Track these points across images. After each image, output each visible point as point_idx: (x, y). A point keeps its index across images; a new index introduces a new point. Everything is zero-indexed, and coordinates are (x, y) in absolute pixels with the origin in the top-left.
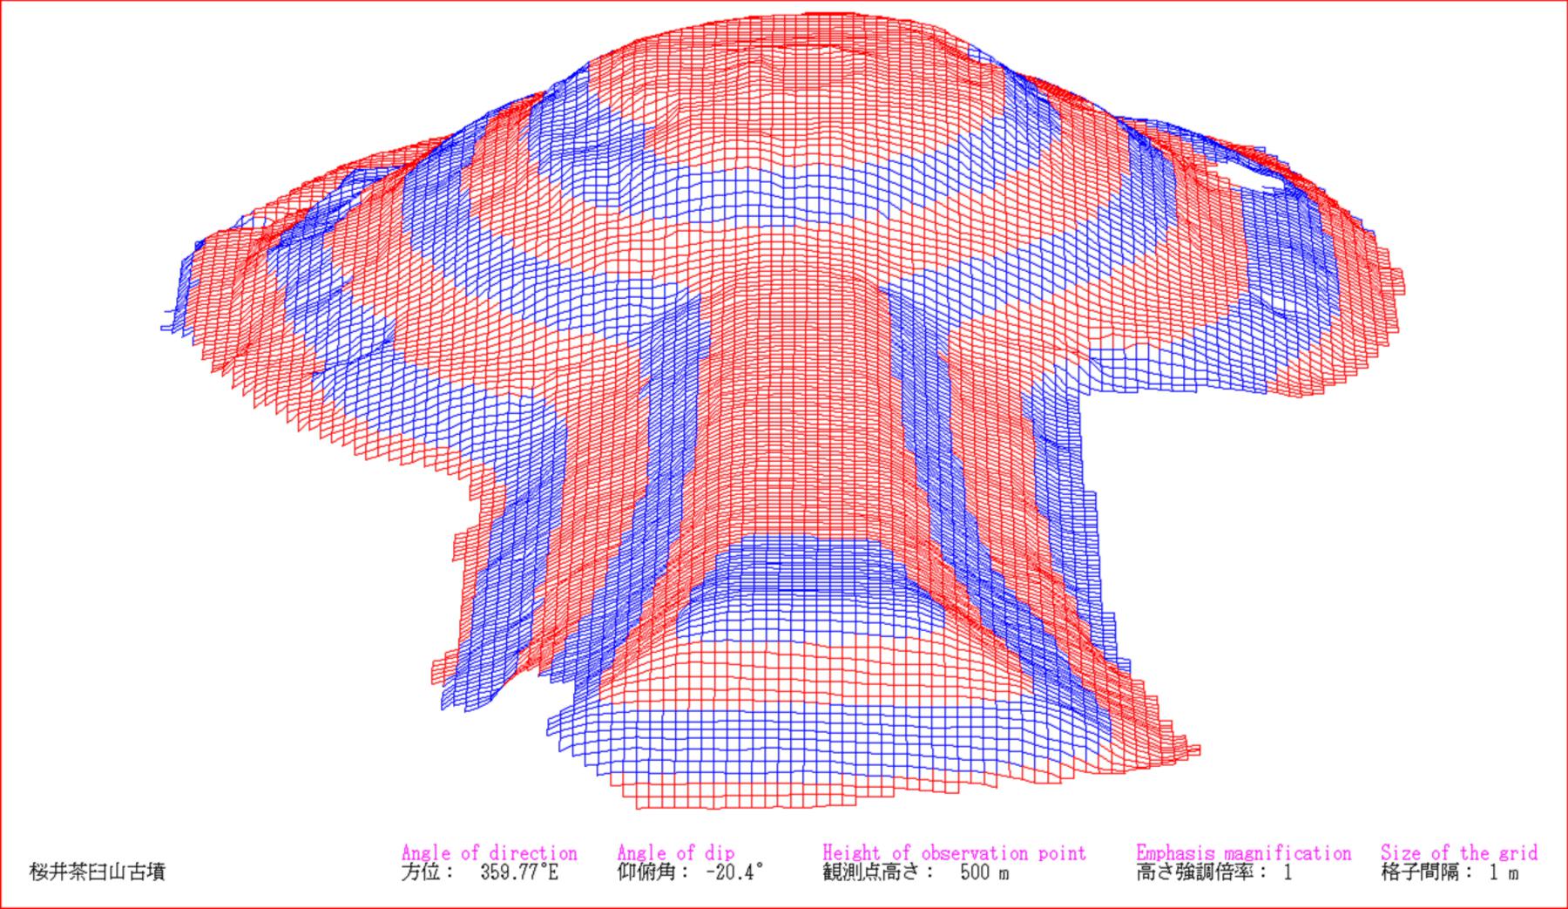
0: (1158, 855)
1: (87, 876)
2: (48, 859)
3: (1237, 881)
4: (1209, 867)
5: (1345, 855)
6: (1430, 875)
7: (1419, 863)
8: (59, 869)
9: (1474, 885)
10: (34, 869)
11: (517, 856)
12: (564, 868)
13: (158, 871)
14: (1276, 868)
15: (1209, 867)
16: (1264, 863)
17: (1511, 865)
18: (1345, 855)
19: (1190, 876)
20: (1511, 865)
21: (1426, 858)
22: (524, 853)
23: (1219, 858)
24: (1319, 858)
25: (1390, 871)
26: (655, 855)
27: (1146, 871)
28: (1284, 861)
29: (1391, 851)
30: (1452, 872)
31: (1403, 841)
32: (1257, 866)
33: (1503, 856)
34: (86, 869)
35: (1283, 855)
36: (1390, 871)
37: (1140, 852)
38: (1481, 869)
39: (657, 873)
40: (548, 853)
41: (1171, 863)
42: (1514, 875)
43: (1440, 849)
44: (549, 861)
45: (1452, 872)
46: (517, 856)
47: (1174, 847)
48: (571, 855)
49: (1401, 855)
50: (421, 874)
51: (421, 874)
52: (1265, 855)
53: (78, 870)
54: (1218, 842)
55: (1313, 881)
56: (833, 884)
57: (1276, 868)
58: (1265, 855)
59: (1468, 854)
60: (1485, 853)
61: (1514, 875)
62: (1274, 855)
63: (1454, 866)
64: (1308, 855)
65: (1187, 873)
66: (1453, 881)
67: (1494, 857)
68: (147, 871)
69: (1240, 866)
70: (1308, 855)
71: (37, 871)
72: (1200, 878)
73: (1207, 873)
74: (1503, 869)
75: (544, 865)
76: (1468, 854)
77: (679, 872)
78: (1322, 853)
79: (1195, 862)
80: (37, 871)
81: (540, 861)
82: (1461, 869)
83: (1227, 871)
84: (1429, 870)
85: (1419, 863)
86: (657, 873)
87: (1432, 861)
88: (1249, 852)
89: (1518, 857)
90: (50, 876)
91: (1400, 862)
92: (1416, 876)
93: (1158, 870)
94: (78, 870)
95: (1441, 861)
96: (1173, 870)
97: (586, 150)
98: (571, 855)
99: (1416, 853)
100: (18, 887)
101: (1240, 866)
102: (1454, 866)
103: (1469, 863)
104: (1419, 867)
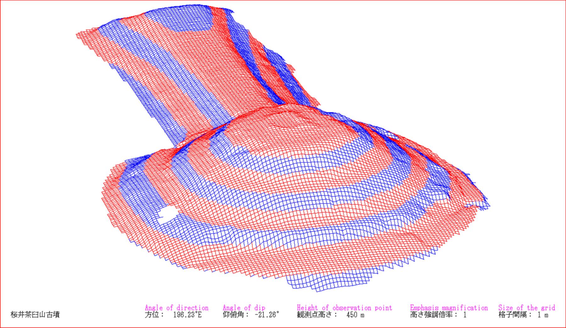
0: (418, 308)
1: (31, 316)
2: (17, 310)
3: (447, 318)
4: (436, 313)
5: (486, 308)
6: (516, 316)
7: (512, 311)
8: (21, 314)
9: (532, 319)
10: (12, 314)
11: (187, 309)
12: (204, 313)
13: (57, 314)
14: (460, 313)
15: (436, 313)
16: (456, 311)
17: (545, 312)
18: (486, 308)
19: (430, 316)
20: (545, 312)
21: (515, 310)
22: (189, 308)
23: (440, 310)
24: (476, 310)
25: (502, 314)
26: (236, 309)
27: (414, 314)
28: (463, 311)
29: (502, 307)
30: (524, 315)
31: (507, 303)
32: (454, 312)
33: (543, 309)
34: (31, 313)
35: (463, 308)
36: (502, 314)
37: (411, 307)
38: (535, 313)
39: (237, 315)
40: (198, 308)
41: (423, 311)
42: (546, 316)
43: (520, 306)
44: (198, 311)
45: (524, 315)
46: (187, 309)
47: (424, 306)
48: (206, 308)
49: (506, 308)
50: (152, 316)
51: (152, 316)
52: (457, 309)
53: (28, 314)
55: (474, 318)
56: (301, 319)
57: (460, 313)
58: (457, 309)
59: (530, 308)
60: (536, 308)
61: (546, 316)
62: (460, 308)
63: (525, 313)
64: (472, 309)
65: (429, 315)
66: (524, 318)
67: (539, 309)
68: (53, 314)
69: (448, 312)
70: (472, 309)
71: (13, 314)
72: (433, 317)
73: (436, 315)
74: (542, 314)
75: (196, 312)
76: (530, 308)
77: (245, 315)
78: (477, 308)
79: (431, 311)
80: (13, 314)
81: (195, 311)
82: (528, 314)
83: (443, 314)
84: (516, 314)
85: (512, 311)
86: (237, 315)
87: (517, 311)
88: (451, 308)
89: (548, 309)
90: (18, 316)
91: (506, 311)
92: (511, 316)
93: (418, 314)
94: (28, 314)
95: (520, 311)
96: (424, 314)
98: (206, 308)
99: (511, 308)
100: (7, 320)
101: (448, 312)
102: (525, 313)
103: (530, 311)
104: (512, 313)
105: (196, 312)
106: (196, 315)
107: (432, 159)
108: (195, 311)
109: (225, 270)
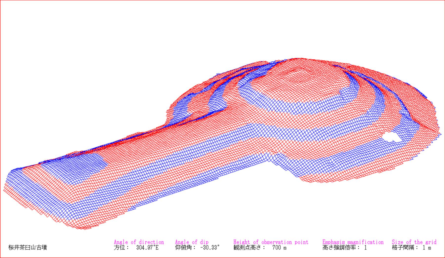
0: (329, 243)
1: (25, 249)
2: (14, 244)
3: (351, 250)
4: (343, 246)
5: (382, 243)
6: (406, 248)
7: (403, 245)
8: (17, 247)
9: (418, 251)
10: (10, 247)
11: (147, 243)
12: (160, 246)
13: (45, 247)
14: (362, 246)
15: (343, 246)
16: (359, 245)
17: (429, 246)
18: (382, 243)
19: (338, 249)
20: (429, 246)
21: (405, 243)
22: (149, 242)
23: (346, 244)
24: (374, 244)
25: (394, 247)
26: (186, 243)
27: (325, 247)
28: (364, 244)
29: (395, 241)
30: (412, 247)
31: (398, 239)
32: (357, 246)
33: (427, 243)
34: (24, 247)
35: (364, 243)
36: (394, 247)
37: (324, 242)
38: (420, 247)
39: (187, 248)
40: (155, 242)
41: (332, 245)
42: (430, 248)
43: (409, 241)
44: (156, 244)
45: (412, 247)
46: (147, 243)
47: (333, 241)
48: (162, 243)
49: (398, 243)
50: (119, 248)
51: (119, 248)
52: (359, 243)
53: (22, 247)
55: (373, 250)
56: (237, 251)
57: (362, 246)
58: (359, 243)
59: (417, 242)
60: (421, 242)
61: (430, 248)
62: (361, 243)
63: (413, 246)
64: (371, 243)
65: (337, 248)
66: (412, 250)
67: (424, 243)
68: (42, 247)
69: (352, 246)
70: (371, 243)
71: (11, 247)
72: (341, 249)
73: (343, 248)
74: (427, 247)
75: (154, 245)
76: (417, 242)
77: (193, 248)
78: (375, 242)
79: (339, 245)
80: (11, 247)
81: (153, 245)
82: (415, 247)
83: (348, 247)
84: (406, 247)
85: (403, 245)
86: (187, 248)
87: (406, 244)
88: (354, 242)
89: (431, 243)
90: (14, 249)
91: (397, 245)
92: (402, 249)
93: (329, 247)
94: (22, 247)
95: (409, 244)
96: (333, 247)
98: (162, 243)
99: (402, 242)
100: (5, 252)
101: (352, 246)
102: (413, 246)
103: (417, 245)
104: (403, 246)
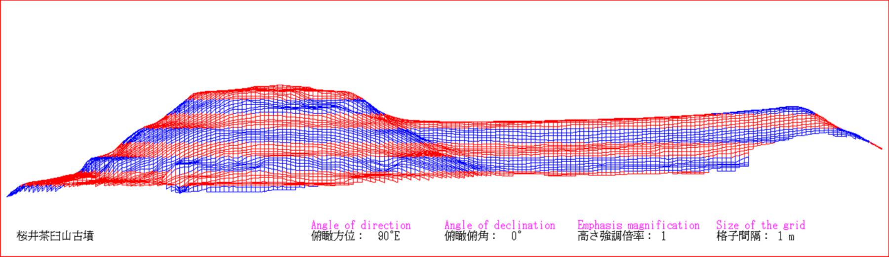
0: (589, 226)
1: (49, 238)
2: (27, 229)
3: (635, 241)
4: (619, 233)
5: (696, 226)
6: (744, 237)
7: (738, 231)
8: (34, 234)
9: (769, 244)
10: (19, 234)
11: (376, 227)
12: (403, 233)
13: (90, 235)
14: (656, 234)
15: (619, 233)
16: (650, 231)
17: (790, 232)
18: (696, 226)
19: (608, 239)
20: (790, 232)
21: (741, 228)
22: (380, 225)
23: (625, 228)
24: (681, 228)
25: (721, 236)
26: (332, 227)
27: (583, 236)
28: (661, 230)
29: (722, 224)
30: (757, 236)
31: (730, 218)
32: (646, 232)
33: (786, 227)
34: (49, 234)
35: (661, 226)
36: (721, 236)
37: (580, 225)
38: (773, 234)
39: (478, 237)
40: (394, 226)
41: (597, 231)
42: (791, 237)
43: (483, 223)
44: (394, 230)
45: (757, 236)
46: (376, 227)
47: (599, 222)
48: (407, 226)
49: (728, 226)
50: (344, 237)
51: (344, 237)
52: (651, 227)
53: (44, 235)
54: (624, 219)
55: (529, 242)
56: (450, 242)
57: (656, 234)
58: (651, 227)
59: (766, 225)
60: (775, 225)
61: (791, 237)
62: (655, 226)
63: (758, 233)
64: (675, 226)
65: (606, 237)
66: (757, 241)
67: (780, 227)
68: (83, 236)
69: (636, 233)
70: (675, 226)
71: (21, 236)
72: (614, 239)
73: (618, 236)
74: (785, 234)
75: (392, 232)
76: (766, 225)
77: (490, 236)
78: (538, 225)
79: (611, 231)
80: (21, 236)
81: (389, 231)
82: (762, 235)
83: (629, 236)
84: (744, 235)
85: (738, 231)
86: (478, 237)
87: (745, 230)
88: (641, 225)
89: (794, 227)
90: (28, 238)
91: (727, 230)
92: (736, 238)
93: (590, 235)
94: (44, 235)
95: (750, 230)
96: (599, 235)
97: (202, 105)
98: (407, 226)
99: (736, 225)
100: (11, 245)
101: (636, 233)
102: (758, 233)
103: (766, 231)
104: (738, 233)
105: (392, 232)
106: (392, 236)
107: (364, 101)
108: (389, 231)
109: (70, 175)
